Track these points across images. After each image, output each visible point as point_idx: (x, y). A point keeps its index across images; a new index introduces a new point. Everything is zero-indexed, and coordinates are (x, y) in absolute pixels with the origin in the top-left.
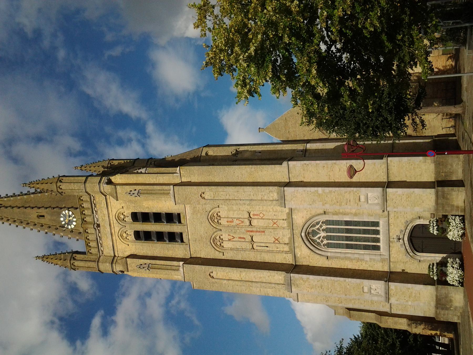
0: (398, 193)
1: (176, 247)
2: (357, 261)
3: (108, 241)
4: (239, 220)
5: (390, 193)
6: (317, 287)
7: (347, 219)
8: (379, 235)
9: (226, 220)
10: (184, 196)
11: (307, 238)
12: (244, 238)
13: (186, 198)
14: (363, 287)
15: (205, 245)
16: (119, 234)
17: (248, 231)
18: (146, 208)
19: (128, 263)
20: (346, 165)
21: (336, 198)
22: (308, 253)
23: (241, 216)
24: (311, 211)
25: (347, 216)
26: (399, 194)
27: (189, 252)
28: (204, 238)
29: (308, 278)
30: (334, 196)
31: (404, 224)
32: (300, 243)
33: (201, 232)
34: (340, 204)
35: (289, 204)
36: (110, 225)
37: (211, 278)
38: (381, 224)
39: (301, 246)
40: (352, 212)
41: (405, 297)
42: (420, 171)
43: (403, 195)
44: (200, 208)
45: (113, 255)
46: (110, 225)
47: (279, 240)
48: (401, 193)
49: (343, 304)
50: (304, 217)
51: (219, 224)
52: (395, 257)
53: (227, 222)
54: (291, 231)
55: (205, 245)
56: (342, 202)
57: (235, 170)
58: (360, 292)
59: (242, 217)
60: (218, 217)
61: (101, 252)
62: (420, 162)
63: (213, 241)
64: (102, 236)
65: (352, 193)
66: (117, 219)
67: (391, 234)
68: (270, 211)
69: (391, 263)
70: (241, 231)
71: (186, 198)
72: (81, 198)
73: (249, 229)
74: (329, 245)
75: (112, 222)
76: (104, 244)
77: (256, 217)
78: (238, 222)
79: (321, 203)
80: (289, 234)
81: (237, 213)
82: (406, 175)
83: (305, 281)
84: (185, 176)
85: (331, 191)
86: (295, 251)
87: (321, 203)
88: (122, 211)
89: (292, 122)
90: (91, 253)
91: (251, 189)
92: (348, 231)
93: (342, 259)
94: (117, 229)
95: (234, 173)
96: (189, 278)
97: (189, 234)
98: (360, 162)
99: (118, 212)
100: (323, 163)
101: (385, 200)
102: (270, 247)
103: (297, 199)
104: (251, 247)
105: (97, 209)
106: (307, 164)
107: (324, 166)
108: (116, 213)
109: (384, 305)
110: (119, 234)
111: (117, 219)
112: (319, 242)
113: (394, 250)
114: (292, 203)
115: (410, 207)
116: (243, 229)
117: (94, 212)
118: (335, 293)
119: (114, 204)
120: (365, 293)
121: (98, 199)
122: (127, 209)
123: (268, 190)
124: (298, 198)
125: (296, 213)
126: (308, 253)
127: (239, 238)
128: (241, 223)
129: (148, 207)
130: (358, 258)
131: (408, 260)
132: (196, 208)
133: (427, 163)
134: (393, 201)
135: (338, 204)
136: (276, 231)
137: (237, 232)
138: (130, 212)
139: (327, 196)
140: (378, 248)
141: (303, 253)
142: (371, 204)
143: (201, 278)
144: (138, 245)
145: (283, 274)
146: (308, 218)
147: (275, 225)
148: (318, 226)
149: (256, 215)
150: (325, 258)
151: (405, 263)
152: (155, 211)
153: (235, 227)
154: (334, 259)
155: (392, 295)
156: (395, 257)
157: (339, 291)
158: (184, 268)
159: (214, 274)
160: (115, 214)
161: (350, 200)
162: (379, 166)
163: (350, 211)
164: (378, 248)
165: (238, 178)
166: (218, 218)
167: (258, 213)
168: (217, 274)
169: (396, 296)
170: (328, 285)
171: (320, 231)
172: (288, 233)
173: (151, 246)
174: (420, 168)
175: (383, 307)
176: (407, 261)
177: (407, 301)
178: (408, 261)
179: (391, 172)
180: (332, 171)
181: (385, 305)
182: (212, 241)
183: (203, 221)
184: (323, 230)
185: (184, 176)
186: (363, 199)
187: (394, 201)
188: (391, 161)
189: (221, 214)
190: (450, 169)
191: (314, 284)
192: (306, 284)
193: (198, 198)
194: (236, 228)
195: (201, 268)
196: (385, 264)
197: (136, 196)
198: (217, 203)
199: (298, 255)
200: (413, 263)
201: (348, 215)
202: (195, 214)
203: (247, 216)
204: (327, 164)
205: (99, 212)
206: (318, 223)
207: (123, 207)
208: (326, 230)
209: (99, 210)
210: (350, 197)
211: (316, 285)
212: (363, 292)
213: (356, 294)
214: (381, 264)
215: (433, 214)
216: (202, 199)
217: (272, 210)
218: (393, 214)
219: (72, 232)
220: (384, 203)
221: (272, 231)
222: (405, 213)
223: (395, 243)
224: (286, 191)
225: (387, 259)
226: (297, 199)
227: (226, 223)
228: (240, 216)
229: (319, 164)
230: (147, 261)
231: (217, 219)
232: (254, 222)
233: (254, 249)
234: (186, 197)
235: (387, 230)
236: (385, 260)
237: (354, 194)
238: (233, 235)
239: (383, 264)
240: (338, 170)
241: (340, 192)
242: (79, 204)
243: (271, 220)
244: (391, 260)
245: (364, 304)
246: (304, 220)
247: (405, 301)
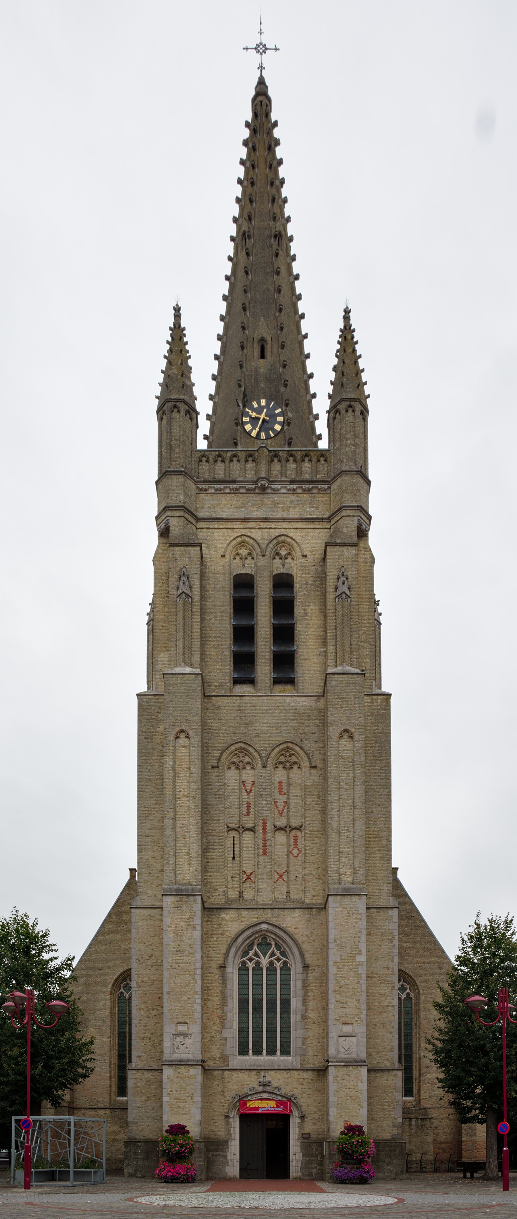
0: (360, 1084)
1: (225, 665)
2: (219, 1016)
3: (229, 509)
4: (284, 806)
5: (360, 1071)
6: (178, 943)
7: (295, 1003)
8: (267, 1055)
9: (284, 780)
10: (344, 695)
11: (257, 932)
12: (248, 814)
13: (340, 698)
14: (187, 1023)
15: (231, 730)
16: (247, 539)
17: (265, 823)
18: (305, 610)
19: (190, 548)
20: (390, 1005)
21: (348, 985)
22: (229, 933)
23: (293, 812)
24: (308, 943)
25: (300, 1004)
26: (357, 1085)
27: (214, 694)
28: (246, 730)
29: (195, 928)
30: (351, 982)
31: (291, 1093)
32: (248, 920)
33: (260, 725)
34: (337, 991)
35: (336, 902)
36: (266, 520)
37: (174, 733)
38: (286, 1058)
39: (242, 922)
40: (309, 1011)
41: (177, 1091)
42: (380, 1118)
43: (357, 1091)
44: (307, 729)
45: (201, 514)
46: (266, 519)
47: (248, 882)
48: (359, 1088)
49: (137, 989)
50: (297, 931)
51: (276, 764)
52: (233, 1078)
53: (280, 783)
54: (268, 904)
55: (231, 730)
56: (340, 994)
57: (384, 808)
58: (177, 1018)
59: (291, 814)
60: (291, 765)
61: (204, 486)
62: (394, 1118)
63: (241, 748)
64: (241, 496)
65: (357, 1011)
66: (280, 539)
67: (272, 1073)
68: (305, 868)
69: (220, 1072)
70: (265, 808)
71: (340, 698)
72: (322, 459)
73: (269, 827)
74: (243, 968)
75: (273, 525)
76: (224, 500)
77: (292, 841)
78: (281, 804)
79: (339, 959)
80: (263, 901)
81: (297, 804)
82: (372, 1098)
83: (189, 922)
84: (373, 704)
85: (361, 978)
86: (232, 910)
87: (339, 959)
88: (297, 553)
89: (406, 927)
90: (201, 461)
91: (360, 833)
92: (271, 1003)
93: (221, 991)
94: (257, 534)
95: (379, 805)
96: (171, 685)
97: (253, 698)
98: (395, 1027)
99: (295, 545)
100: (394, 967)
101: (347, 1064)
102: (233, 863)
103: (346, 918)
104: (232, 826)
105: (300, 495)
106: (394, 941)
107: (388, 969)
108: (291, 538)
109: (142, 1058)
110: (247, 539)
111: (280, 539)
112: (249, 953)
113: (246, 1077)
114: (338, 908)
115: (336, 1101)
116: (268, 813)
117: (295, 486)
118: (170, 975)
119: (312, 538)
120: (176, 1026)
121: (320, 499)
122: (302, 566)
123: (359, 865)
124: (347, 919)
125: (304, 916)
126: (229, 933)
127: (248, 804)
128: (279, 811)
129: (306, 615)
130: (226, 1019)
131: (228, 1098)
132: (309, 720)
133: (391, 1129)
134: (346, 1076)
135: (338, 988)
136: (266, 876)
137: (263, 800)
138: (295, 571)
139: (351, 970)
140: (243, 1051)
141: (230, 924)
142: (338, 1041)
143: (173, 712)
144: (224, 579)
145: (196, 882)
146: (296, 936)
147: (277, 876)
148: (278, 953)
149: (296, 842)
150: (221, 962)
151: (222, 1093)
152: (299, 628)
153: (271, 796)
154: (221, 978)
155: (178, 1071)
156: (233, 1078)
157: (174, 982)
158: (193, 676)
159: (182, 741)
160: (290, 535)
161: (345, 1008)
162: (388, 1057)
163: (310, 1008)
164: (243, 1051)
165: (370, 811)
166: (288, 764)
167: (300, 846)
168: (184, 746)
169: (177, 1077)
170: (185, 963)
171: (270, 958)
172: (264, 899)
173: (223, 609)
174: (384, 1118)
175: (138, 1056)
176: (225, 1097)
177: (170, 1094)
178: (227, 1099)
179: (378, 1075)
180: (381, 983)
181: (142, 1061)
182: (240, 745)
183: (281, 732)
184: (271, 963)
185: (372, 702)
186: (347, 1029)
187: (347, 1078)
188: (396, 1075)
189: (296, 771)
190: (384, 1161)
191: (184, 938)
192: (183, 924)
193: (342, 725)
194: (269, 799)
195: (195, 714)
196: (218, 1062)
197: (336, 588)
198: (332, 763)
199: (223, 915)
200: (223, 1106)
201: (303, 1005)
202: (295, 716)
203: (294, 822)
204: (393, 973)
205: (293, 498)
206: (283, 954)
207: (306, 556)
208: (271, 968)
209: (298, 498)
210: (350, 1008)
211: (183, 941)
212: (178, 1023)
213: (171, 1010)
214: (218, 1056)
215: (310, 1137)
216: (339, 732)
217: (307, 872)
218: (307, 1077)
219: (237, 424)
220: (342, 1062)
221: (268, 870)
222: (309, 1094)
223: (258, 1078)
224: (359, 899)
225: (228, 1065)
226: (346, 918)
227: (278, 780)
228: (293, 810)
229: (393, 961)
230: (196, 593)
231: (286, 762)
232: (281, 838)
233: (229, 831)
234: (343, 698)
235: (279, 1066)
236: (224, 1062)
237: (356, 1014)
238: (253, 792)
239: (218, 1059)
240: (382, 992)
241: (358, 992)
242: (310, 450)
243: (286, 869)
244: (226, 1073)
245: (141, 1026)
246: (290, 929)
247: (169, 1091)
